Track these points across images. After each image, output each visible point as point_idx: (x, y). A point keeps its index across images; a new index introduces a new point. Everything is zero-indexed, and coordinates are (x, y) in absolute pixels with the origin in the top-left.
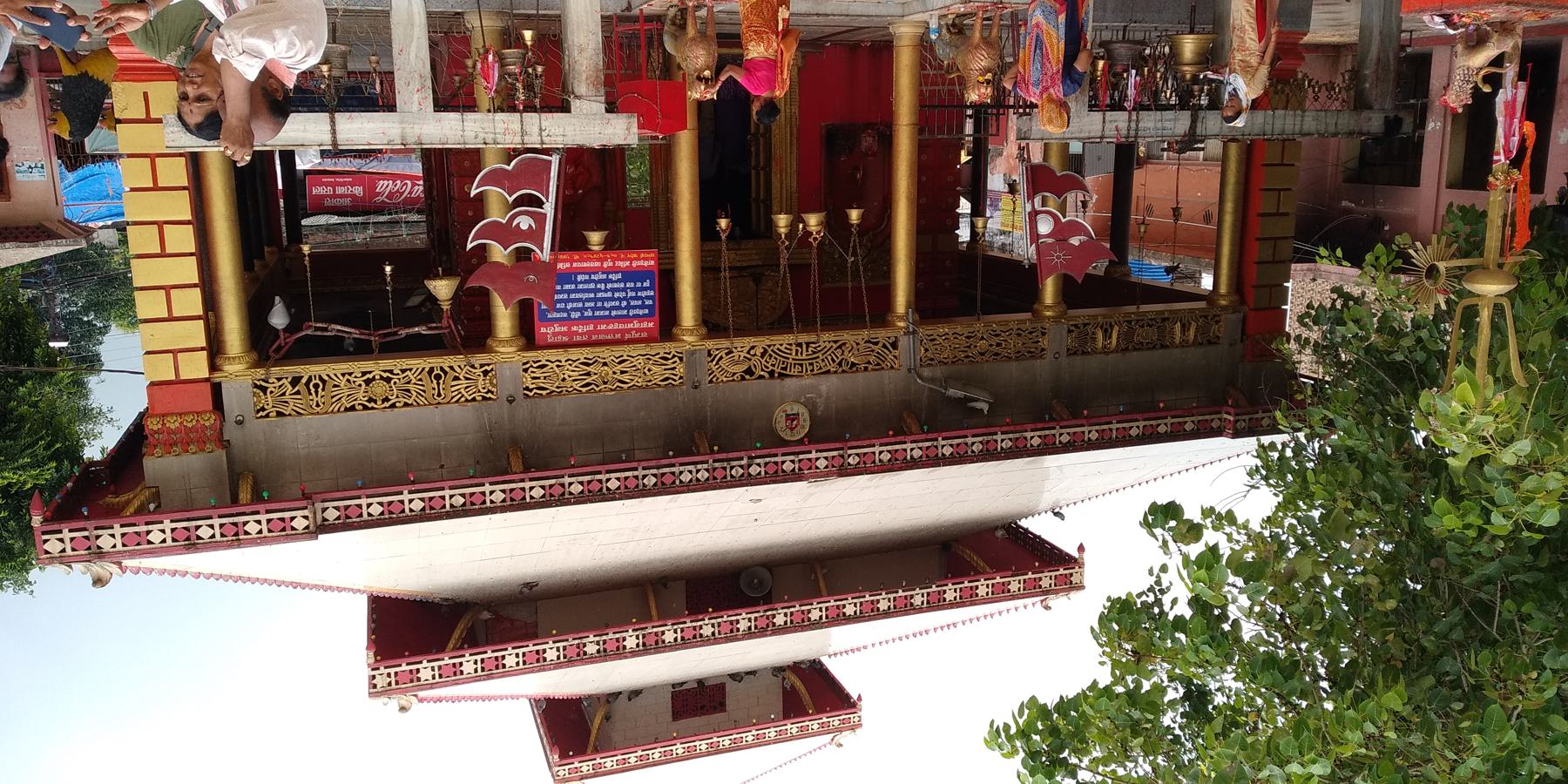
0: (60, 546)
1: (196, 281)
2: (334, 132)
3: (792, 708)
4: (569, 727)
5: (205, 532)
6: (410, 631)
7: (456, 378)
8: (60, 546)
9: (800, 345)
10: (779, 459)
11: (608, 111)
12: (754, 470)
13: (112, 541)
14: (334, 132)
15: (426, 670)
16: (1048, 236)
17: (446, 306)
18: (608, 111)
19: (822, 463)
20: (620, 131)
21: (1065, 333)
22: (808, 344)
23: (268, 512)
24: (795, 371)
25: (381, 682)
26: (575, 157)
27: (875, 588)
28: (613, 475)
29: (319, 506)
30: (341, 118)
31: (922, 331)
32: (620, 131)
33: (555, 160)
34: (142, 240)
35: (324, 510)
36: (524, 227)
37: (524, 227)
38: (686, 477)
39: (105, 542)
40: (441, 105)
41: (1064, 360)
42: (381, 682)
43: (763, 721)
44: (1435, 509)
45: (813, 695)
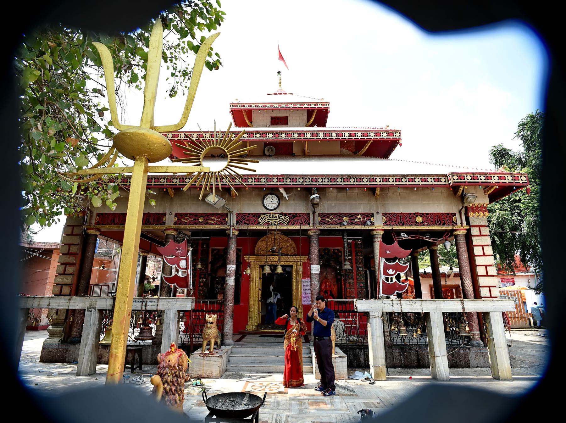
0: (522, 178)
1: (476, 258)
2: (463, 305)
3: (249, 112)
4: (318, 115)
5: (483, 178)
6: (382, 146)
7: (395, 221)
8: (522, 178)
9: (274, 225)
10: (292, 183)
11: (369, 312)
12: (301, 180)
13: (508, 178)
14: (463, 305)
15: (385, 135)
16: (181, 259)
18: (369, 312)
19: (275, 180)
20: (361, 305)
21: (166, 222)
22: (272, 225)
23: (465, 182)
24: (276, 215)
25: (398, 134)
26: (374, 296)
28: (352, 183)
29: (447, 183)
30: (460, 310)
31: (226, 227)
32: (361, 305)
33: (381, 294)
34: (493, 271)
35: (445, 182)
36: (391, 270)
37: (391, 270)
38: (326, 180)
39: (510, 178)
40: (427, 314)
41: (168, 212)
42: (398, 134)
44: (184, 68)
45: (242, 115)
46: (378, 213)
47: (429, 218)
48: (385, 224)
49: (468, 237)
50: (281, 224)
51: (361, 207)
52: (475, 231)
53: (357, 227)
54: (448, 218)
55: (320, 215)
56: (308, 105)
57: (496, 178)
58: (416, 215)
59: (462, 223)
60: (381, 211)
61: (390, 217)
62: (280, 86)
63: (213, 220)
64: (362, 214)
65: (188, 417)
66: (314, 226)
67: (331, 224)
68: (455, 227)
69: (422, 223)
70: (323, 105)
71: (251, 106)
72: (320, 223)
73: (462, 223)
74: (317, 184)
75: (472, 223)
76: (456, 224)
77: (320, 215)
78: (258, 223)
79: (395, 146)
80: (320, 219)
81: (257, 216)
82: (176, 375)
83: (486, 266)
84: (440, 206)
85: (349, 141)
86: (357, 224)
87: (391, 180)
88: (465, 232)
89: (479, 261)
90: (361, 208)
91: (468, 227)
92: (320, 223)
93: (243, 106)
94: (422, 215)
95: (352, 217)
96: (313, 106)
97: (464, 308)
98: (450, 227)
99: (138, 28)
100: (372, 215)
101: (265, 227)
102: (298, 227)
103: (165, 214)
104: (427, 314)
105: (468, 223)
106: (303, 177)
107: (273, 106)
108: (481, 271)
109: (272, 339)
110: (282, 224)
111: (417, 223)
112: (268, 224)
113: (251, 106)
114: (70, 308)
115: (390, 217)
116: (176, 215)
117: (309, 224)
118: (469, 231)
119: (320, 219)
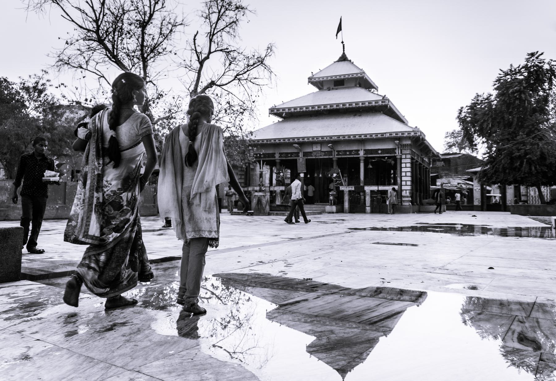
40: (387, 191)
47: (384, 151)
49: (401, 159)
50: (321, 156)
51: (355, 148)
52: (404, 156)
53: (352, 156)
54: (393, 151)
55: (337, 151)
58: (379, 150)
60: (363, 149)
61: (367, 151)
64: (355, 150)
66: (335, 157)
69: (381, 153)
72: (337, 155)
75: (403, 153)
77: (337, 151)
81: (311, 153)
82: (56, 113)
89: (403, 170)
90: (355, 148)
92: (337, 155)
94: (381, 150)
95: (351, 151)
99: (109, 147)
100: (359, 150)
103: (275, 153)
104: (387, 191)
105: (401, 153)
106: (327, 137)
109: (248, 179)
111: (378, 154)
112: (315, 156)
114: (538, 301)
115: (367, 151)
116: (279, 153)
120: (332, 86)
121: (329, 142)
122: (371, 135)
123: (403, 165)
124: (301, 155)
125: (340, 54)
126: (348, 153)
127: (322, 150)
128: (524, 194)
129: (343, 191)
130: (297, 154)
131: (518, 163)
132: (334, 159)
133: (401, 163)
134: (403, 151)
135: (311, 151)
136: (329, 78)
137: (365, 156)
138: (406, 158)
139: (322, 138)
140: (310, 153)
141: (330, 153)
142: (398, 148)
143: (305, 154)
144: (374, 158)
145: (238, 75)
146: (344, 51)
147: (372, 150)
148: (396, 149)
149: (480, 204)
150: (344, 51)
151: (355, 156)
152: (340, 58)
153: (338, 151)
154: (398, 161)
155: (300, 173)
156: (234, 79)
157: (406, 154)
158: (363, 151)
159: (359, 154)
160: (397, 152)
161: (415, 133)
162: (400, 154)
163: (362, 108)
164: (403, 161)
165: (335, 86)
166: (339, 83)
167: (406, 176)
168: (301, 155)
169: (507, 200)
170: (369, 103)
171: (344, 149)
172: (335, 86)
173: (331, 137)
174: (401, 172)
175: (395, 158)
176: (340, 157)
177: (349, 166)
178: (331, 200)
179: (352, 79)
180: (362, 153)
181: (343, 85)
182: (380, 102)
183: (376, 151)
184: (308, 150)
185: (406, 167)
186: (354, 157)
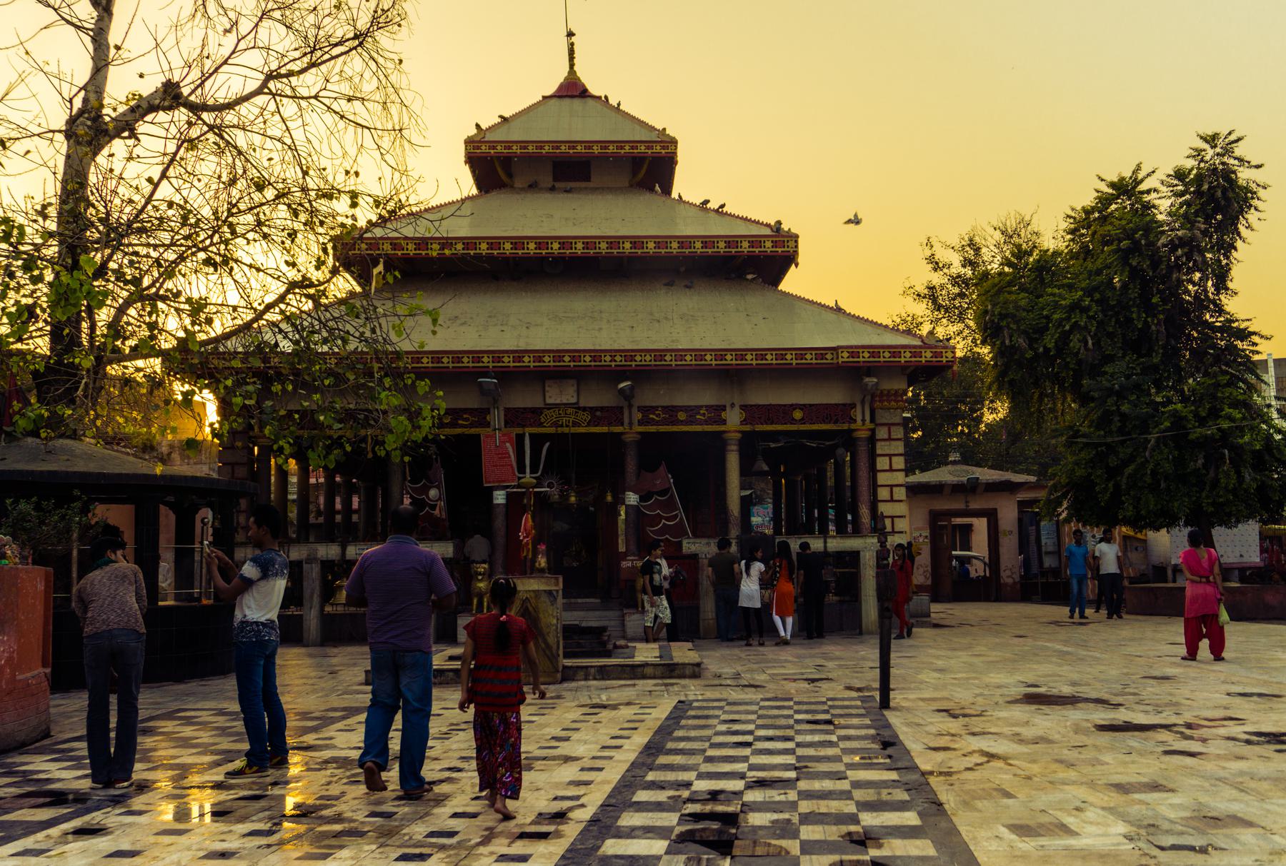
3: (507, 161)
17: (760, 457)
27: (490, 258)
43: (603, 158)
46: (733, 405)
47: (812, 412)
48: (743, 422)
49: (872, 440)
50: (575, 424)
51: (704, 397)
52: (882, 433)
53: (698, 428)
54: (843, 412)
56: (632, 148)
57: (908, 354)
58: (794, 407)
59: (863, 420)
60: (738, 402)
61: (751, 413)
62: (570, 34)
63: (466, 420)
65: (764, 282)
66: (631, 428)
67: (657, 423)
68: (853, 426)
69: (802, 421)
70: (663, 148)
71: (510, 148)
72: (641, 423)
73: (863, 420)
74: (633, 363)
76: (855, 421)
78: (541, 425)
79: (788, 267)
80: (640, 416)
81: (536, 412)
83: (891, 486)
84: (832, 395)
85: (704, 257)
86: (700, 423)
87: (749, 357)
88: (868, 433)
89: (882, 478)
91: (872, 426)
93: (494, 148)
94: (803, 407)
96: (642, 149)
97: (825, 547)
98: (845, 427)
100: (723, 408)
101: (552, 430)
102: (605, 429)
105: (873, 420)
107: (558, 148)
108: (883, 493)
110: (579, 425)
111: (793, 421)
112: (556, 425)
113: (510, 148)
115: (751, 413)
117: (622, 424)
118: (873, 431)
119: (640, 416)
120: (547, 180)
121: (621, 374)
122: (761, 353)
123: (882, 463)
124: (497, 418)
125: (561, 74)
126: (798, 415)
127: (582, 404)
128: (1051, 549)
129: (694, 557)
130: (480, 416)
131: (1200, 462)
132: (628, 438)
133: (873, 456)
134: (879, 413)
135: (539, 404)
136: (547, 149)
137: (747, 428)
138: (890, 439)
139: (594, 359)
140: (534, 415)
141: (612, 414)
142: (863, 402)
143: (515, 417)
144: (773, 436)
145: (270, 76)
146: (572, 66)
147: (769, 408)
148: (853, 406)
149: (929, 582)
150: (572, 66)
151: (663, 429)
152: (561, 87)
153: (646, 410)
154: (863, 450)
155: (491, 490)
156: (258, 92)
157: (889, 425)
158: (737, 409)
159: (724, 422)
160: (859, 418)
161: (936, 355)
162: (869, 425)
163: (656, 258)
164: (881, 448)
165: (556, 179)
166: (570, 169)
167: (892, 500)
168: (497, 418)
169: (1003, 567)
170: (728, 244)
171: (666, 402)
172: (556, 179)
173: (629, 354)
174: (874, 486)
175: (848, 440)
176: (652, 429)
177: (687, 462)
178: (481, 596)
179: (618, 158)
180: (733, 420)
181: (588, 179)
182: (769, 244)
183: (783, 412)
184: (523, 399)
185: (891, 470)
186: (658, 434)
